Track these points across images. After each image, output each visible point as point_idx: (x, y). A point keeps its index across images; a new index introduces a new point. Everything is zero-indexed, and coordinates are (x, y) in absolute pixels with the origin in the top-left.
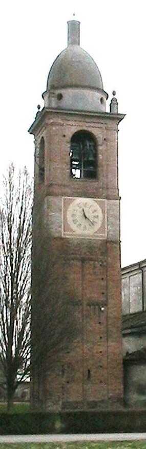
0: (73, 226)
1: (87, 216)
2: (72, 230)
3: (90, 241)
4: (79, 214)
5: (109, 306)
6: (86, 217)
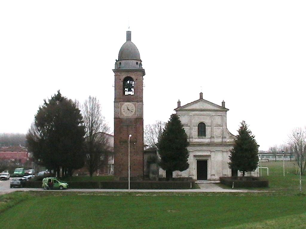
0: (124, 113)
1: (129, 109)
2: (123, 115)
3: (130, 119)
4: (126, 109)
5: (138, 142)
6: (129, 110)
